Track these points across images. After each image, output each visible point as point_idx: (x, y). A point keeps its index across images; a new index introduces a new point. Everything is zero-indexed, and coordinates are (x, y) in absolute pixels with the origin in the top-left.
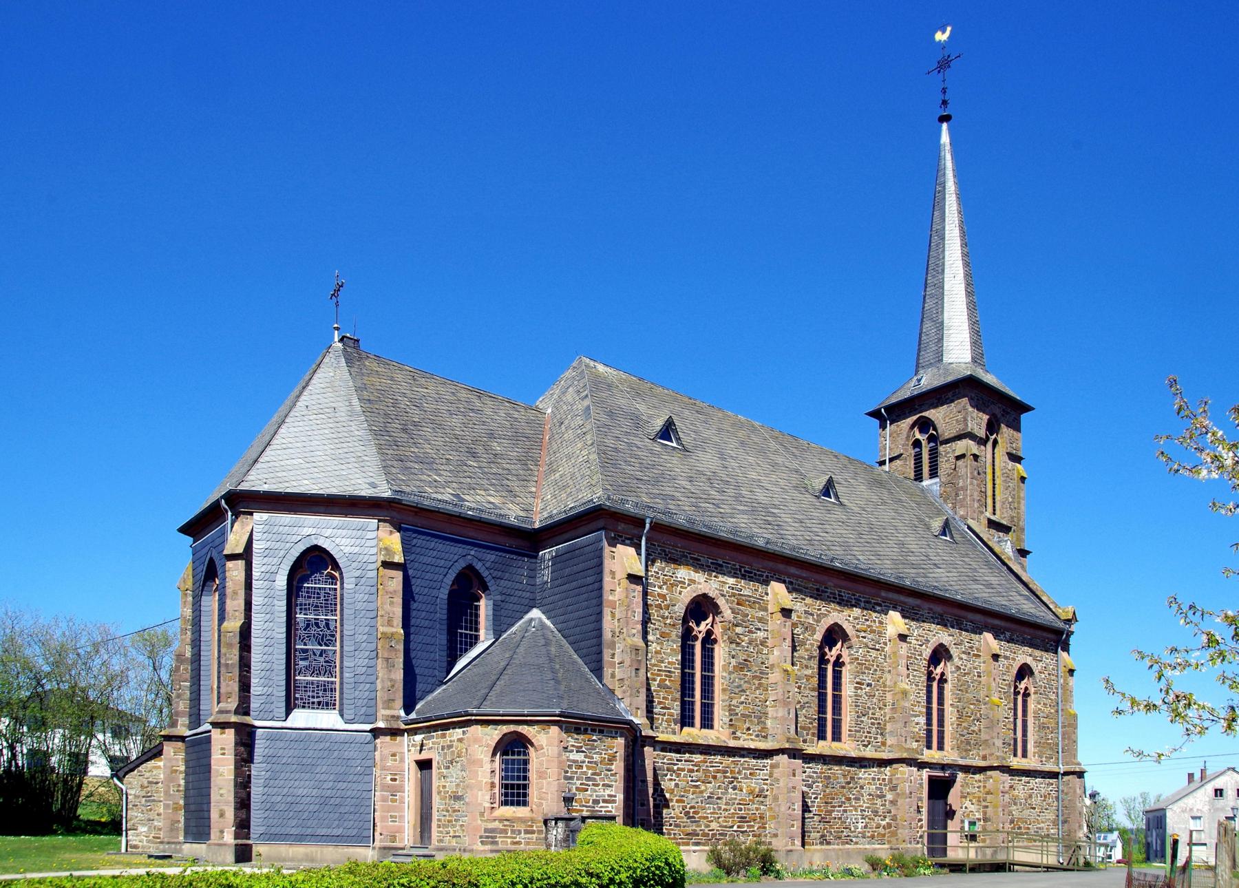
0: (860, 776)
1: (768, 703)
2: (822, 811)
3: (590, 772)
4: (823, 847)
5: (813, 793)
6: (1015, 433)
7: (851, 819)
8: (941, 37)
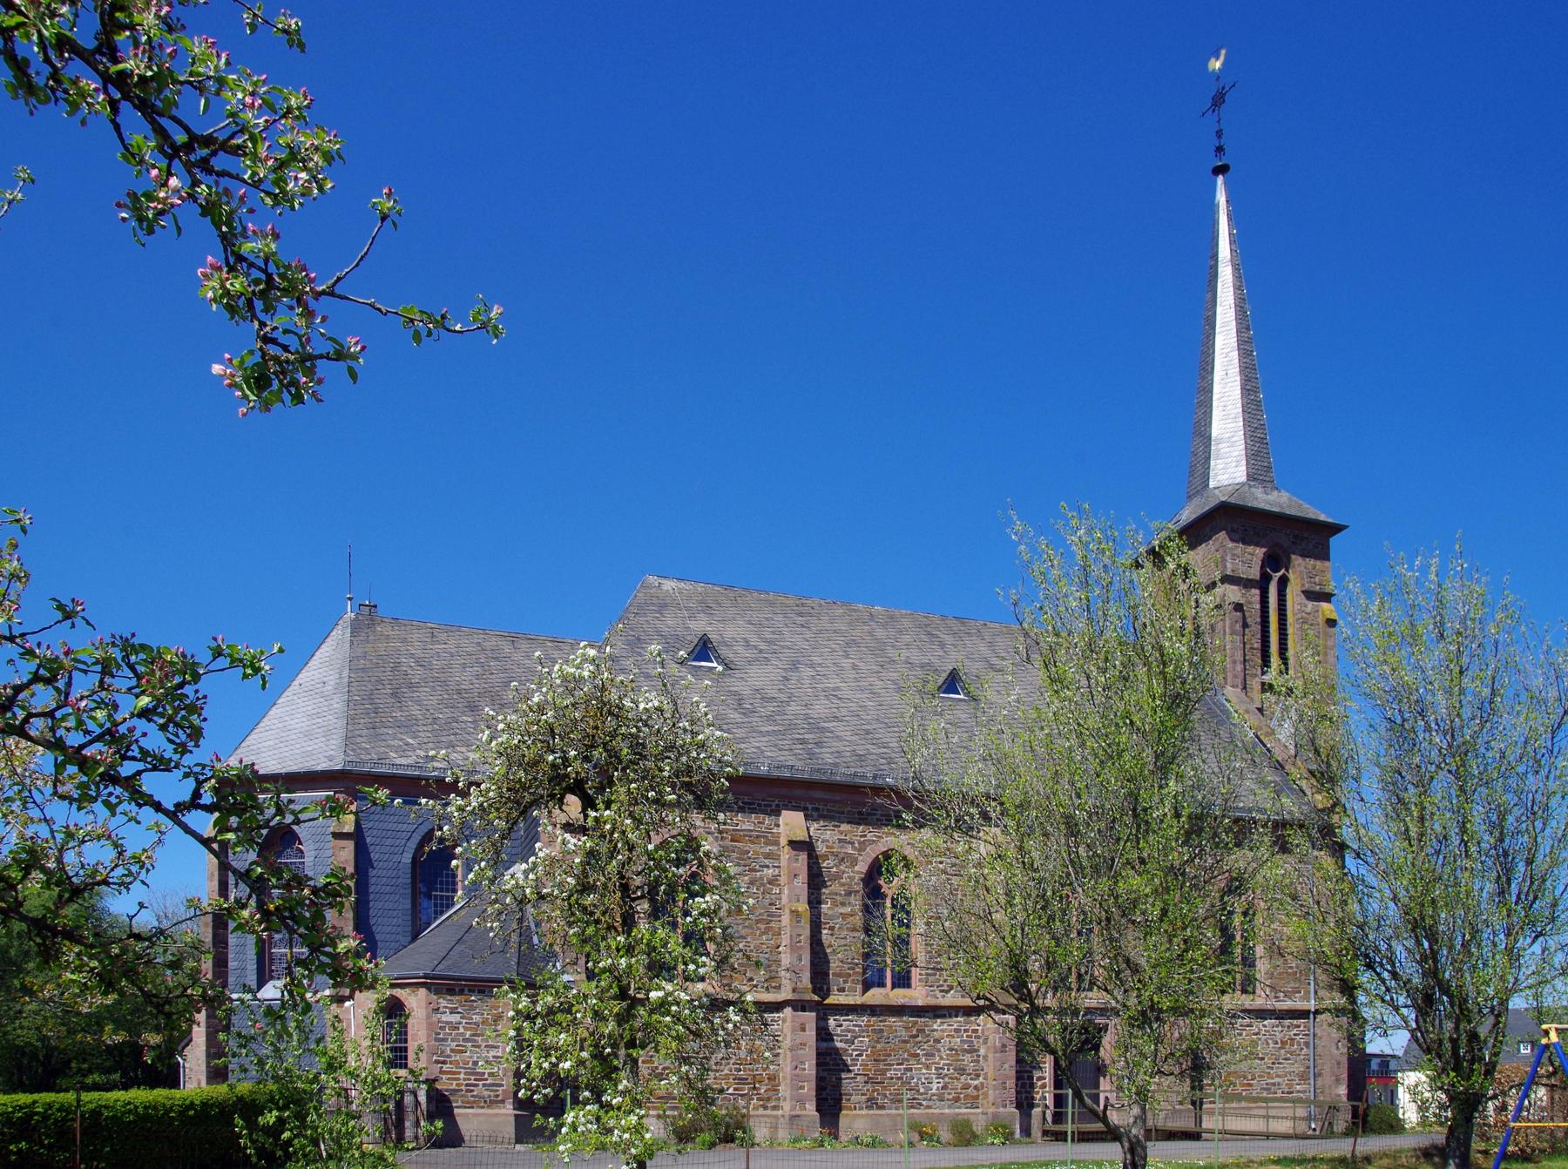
0: (935, 1027)
1: (780, 949)
2: (870, 1070)
3: (469, 1033)
4: (871, 1112)
5: (853, 1050)
6: (1318, 563)
7: (919, 1079)
8: (1216, 65)
